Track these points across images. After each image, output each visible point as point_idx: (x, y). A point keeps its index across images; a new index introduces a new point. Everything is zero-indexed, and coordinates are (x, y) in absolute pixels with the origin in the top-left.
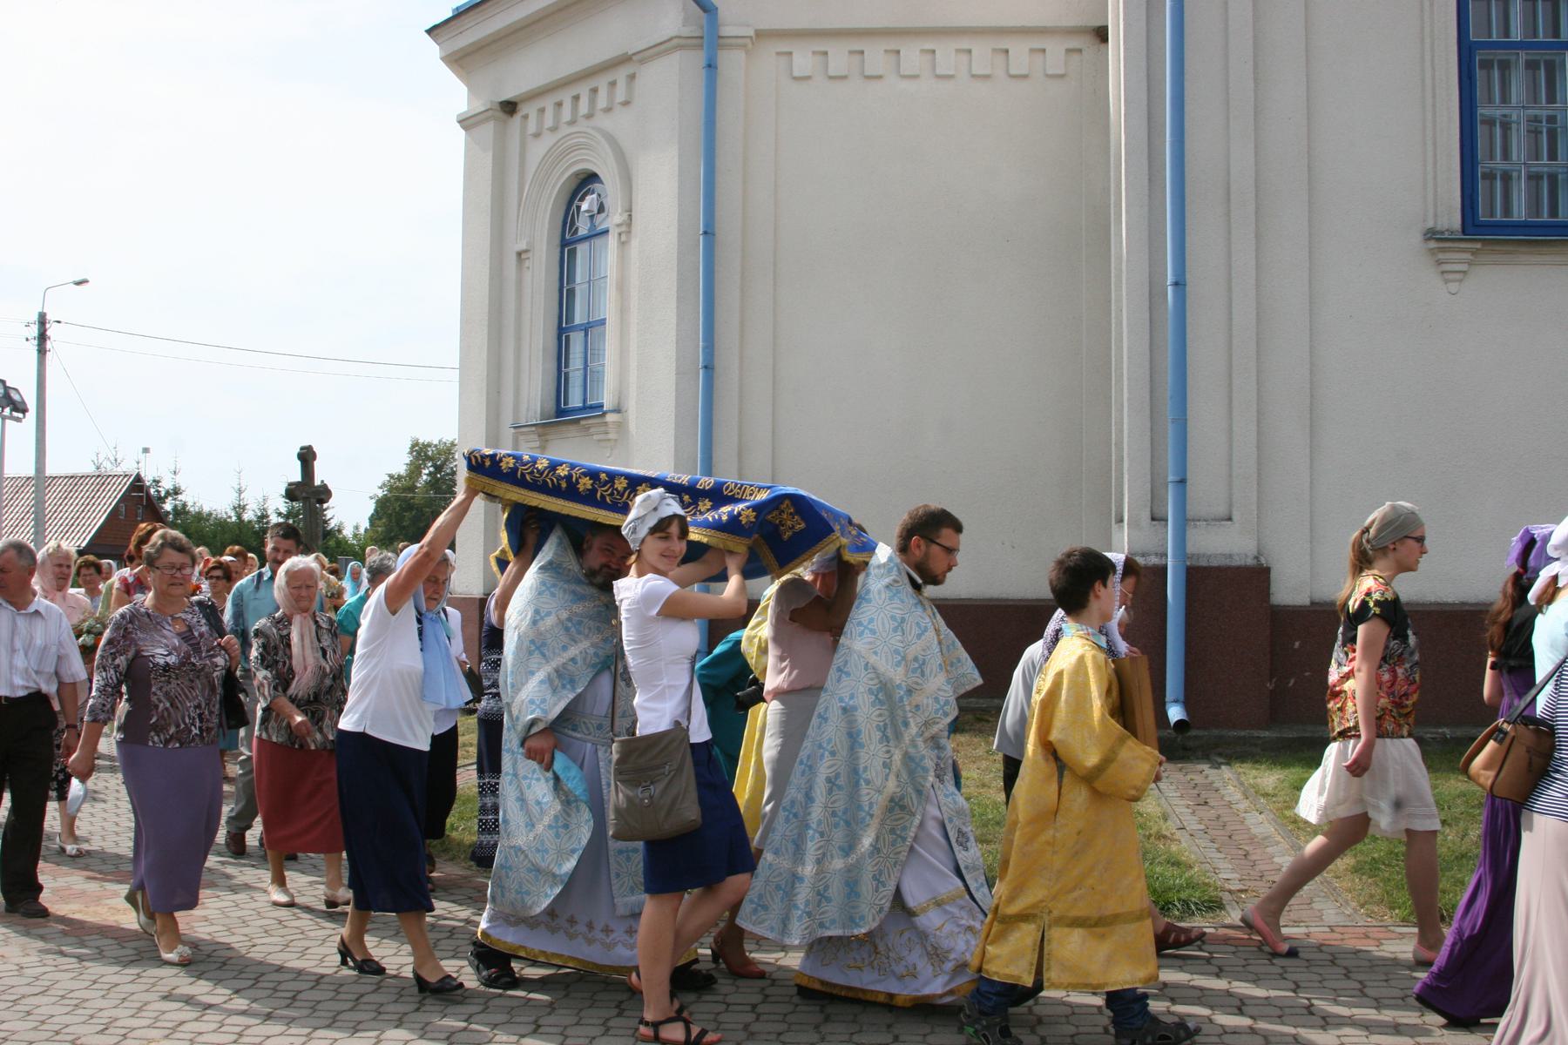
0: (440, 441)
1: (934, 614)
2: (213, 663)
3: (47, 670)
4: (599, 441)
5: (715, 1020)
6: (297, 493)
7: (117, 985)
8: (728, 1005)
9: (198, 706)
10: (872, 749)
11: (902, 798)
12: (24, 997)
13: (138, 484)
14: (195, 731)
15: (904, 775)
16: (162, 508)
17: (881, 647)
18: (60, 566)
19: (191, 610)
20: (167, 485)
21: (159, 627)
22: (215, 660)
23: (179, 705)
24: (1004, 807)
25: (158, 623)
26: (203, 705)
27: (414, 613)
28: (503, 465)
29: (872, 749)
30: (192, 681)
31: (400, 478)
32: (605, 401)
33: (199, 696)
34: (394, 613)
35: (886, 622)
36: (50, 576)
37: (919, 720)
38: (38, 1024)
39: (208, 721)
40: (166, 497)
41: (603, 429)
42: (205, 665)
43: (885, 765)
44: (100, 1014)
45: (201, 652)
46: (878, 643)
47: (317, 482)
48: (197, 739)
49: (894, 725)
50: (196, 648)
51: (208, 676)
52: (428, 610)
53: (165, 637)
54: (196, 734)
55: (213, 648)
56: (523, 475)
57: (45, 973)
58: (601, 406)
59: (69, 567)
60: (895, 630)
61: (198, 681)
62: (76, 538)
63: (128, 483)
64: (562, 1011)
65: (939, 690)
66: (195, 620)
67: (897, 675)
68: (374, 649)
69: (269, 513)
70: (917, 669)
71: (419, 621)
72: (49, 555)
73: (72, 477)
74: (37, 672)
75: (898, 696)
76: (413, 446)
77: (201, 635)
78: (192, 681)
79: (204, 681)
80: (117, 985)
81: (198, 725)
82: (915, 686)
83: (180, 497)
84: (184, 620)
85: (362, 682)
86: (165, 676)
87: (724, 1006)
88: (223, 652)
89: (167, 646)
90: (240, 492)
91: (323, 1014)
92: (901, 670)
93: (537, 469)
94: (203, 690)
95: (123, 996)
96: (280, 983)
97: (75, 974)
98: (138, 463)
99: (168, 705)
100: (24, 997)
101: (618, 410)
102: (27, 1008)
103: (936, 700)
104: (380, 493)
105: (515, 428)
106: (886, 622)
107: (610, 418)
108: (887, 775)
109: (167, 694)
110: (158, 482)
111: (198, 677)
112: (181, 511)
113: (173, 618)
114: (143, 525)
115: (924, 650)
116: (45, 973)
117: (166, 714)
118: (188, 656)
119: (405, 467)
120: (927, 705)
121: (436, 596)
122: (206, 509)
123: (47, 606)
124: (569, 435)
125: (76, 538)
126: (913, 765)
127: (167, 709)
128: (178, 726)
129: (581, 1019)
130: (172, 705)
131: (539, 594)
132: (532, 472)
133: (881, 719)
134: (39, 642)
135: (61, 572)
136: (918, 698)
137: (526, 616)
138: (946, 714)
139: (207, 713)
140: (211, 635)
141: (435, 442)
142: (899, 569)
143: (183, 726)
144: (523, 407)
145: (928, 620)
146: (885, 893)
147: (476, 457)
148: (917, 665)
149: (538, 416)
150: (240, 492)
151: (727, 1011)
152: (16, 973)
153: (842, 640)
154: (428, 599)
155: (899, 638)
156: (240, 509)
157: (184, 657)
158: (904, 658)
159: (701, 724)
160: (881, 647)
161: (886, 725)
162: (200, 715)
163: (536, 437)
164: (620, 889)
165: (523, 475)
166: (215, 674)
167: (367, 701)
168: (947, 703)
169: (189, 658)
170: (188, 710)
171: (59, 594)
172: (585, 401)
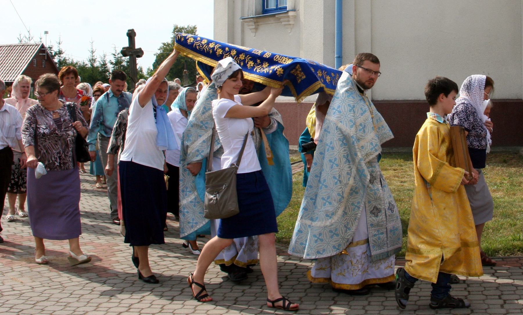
0: (188, 26)
1: (370, 105)
2: (67, 134)
3: (11, 136)
4: (285, 25)
5: (382, 305)
6: (127, 53)
7: (83, 295)
8: (387, 298)
9: (59, 153)
10: (342, 166)
11: (356, 188)
12: (38, 302)
13: (43, 49)
14: (57, 164)
15: (358, 177)
16: (54, 61)
17: (343, 119)
18: (24, 87)
19: (63, 109)
20: (55, 49)
21: (46, 116)
22: (68, 132)
23: (50, 152)
24: (301, 186)
25: (46, 114)
26: (62, 152)
27: (152, 107)
28: (189, 41)
29: (342, 166)
30: (57, 141)
31: (168, 45)
32: (287, 6)
33: (59, 148)
34: (143, 106)
35: (346, 107)
36: (19, 91)
37: (363, 153)
38: (9, 309)
39: (64, 159)
40: (55, 55)
41: (287, 19)
42: (63, 134)
43: (348, 173)
44: (78, 310)
45: (62, 129)
46: (342, 117)
47: (137, 47)
48: (58, 168)
49: (351, 155)
50: (59, 127)
51: (65, 140)
52: (159, 105)
53: (48, 120)
54: (57, 165)
55: (68, 127)
56: (196, 46)
57: (45, 290)
58: (286, 8)
59: (28, 87)
60: (350, 111)
61: (59, 142)
62: (10, 76)
63: (38, 49)
64: (306, 303)
65: (372, 139)
66: (64, 113)
67: (351, 131)
68: (134, 123)
69: (107, 62)
70: (361, 129)
71: (155, 110)
72: (19, 82)
73: (10, 46)
74: (7, 138)
75: (352, 141)
76: (175, 29)
77: (65, 121)
78: (57, 141)
79: (63, 141)
80: (83, 295)
81: (58, 161)
82: (361, 137)
83: (62, 55)
84: (59, 113)
85: (130, 138)
86: (43, 138)
87: (292, 290)
88: (73, 129)
89: (47, 124)
90: (93, 52)
91: (188, 307)
92: (353, 129)
93: (202, 44)
94: (62, 146)
95: (88, 300)
96: (163, 292)
97: (60, 290)
98: (41, 39)
99: (45, 151)
100: (38, 302)
101: (294, 10)
102: (41, 308)
103: (372, 144)
104: (159, 52)
105: (242, 19)
106: (346, 107)
107: (291, 14)
108: (349, 178)
109: (44, 146)
110: (51, 48)
111: (60, 140)
112: (62, 63)
113: (54, 112)
114: (64, 67)
115: (364, 121)
116: (45, 290)
117: (44, 156)
118: (55, 130)
119: (171, 39)
120: (367, 146)
121: (162, 98)
122: (75, 61)
123: (10, 107)
124: (270, 22)
125: (10, 76)
126: (360, 174)
127: (44, 153)
128: (49, 161)
129: (317, 306)
130: (47, 151)
131: (206, 100)
132: (199, 45)
133: (345, 152)
134: (7, 124)
135: (25, 90)
136: (362, 143)
137: (200, 109)
138: (376, 150)
139: (63, 156)
140: (70, 121)
141: (186, 27)
142: (352, 83)
143: (51, 161)
144: (246, 9)
145: (366, 107)
146: (350, 233)
147: (178, 37)
148: (361, 128)
149: (254, 13)
150: (93, 52)
151: (386, 300)
152: (31, 291)
153: (327, 116)
154: (158, 100)
155: (352, 114)
156: (93, 61)
157: (52, 131)
158: (355, 124)
159: (251, 156)
160: (343, 119)
161: (348, 155)
162: (60, 157)
163: (253, 24)
164: (335, 242)
165: (196, 46)
166: (68, 139)
167: (133, 148)
168: (376, 145)
169: (55, 131)
170: (54, 154)
171: (23, 100)
172: (277, 5)
